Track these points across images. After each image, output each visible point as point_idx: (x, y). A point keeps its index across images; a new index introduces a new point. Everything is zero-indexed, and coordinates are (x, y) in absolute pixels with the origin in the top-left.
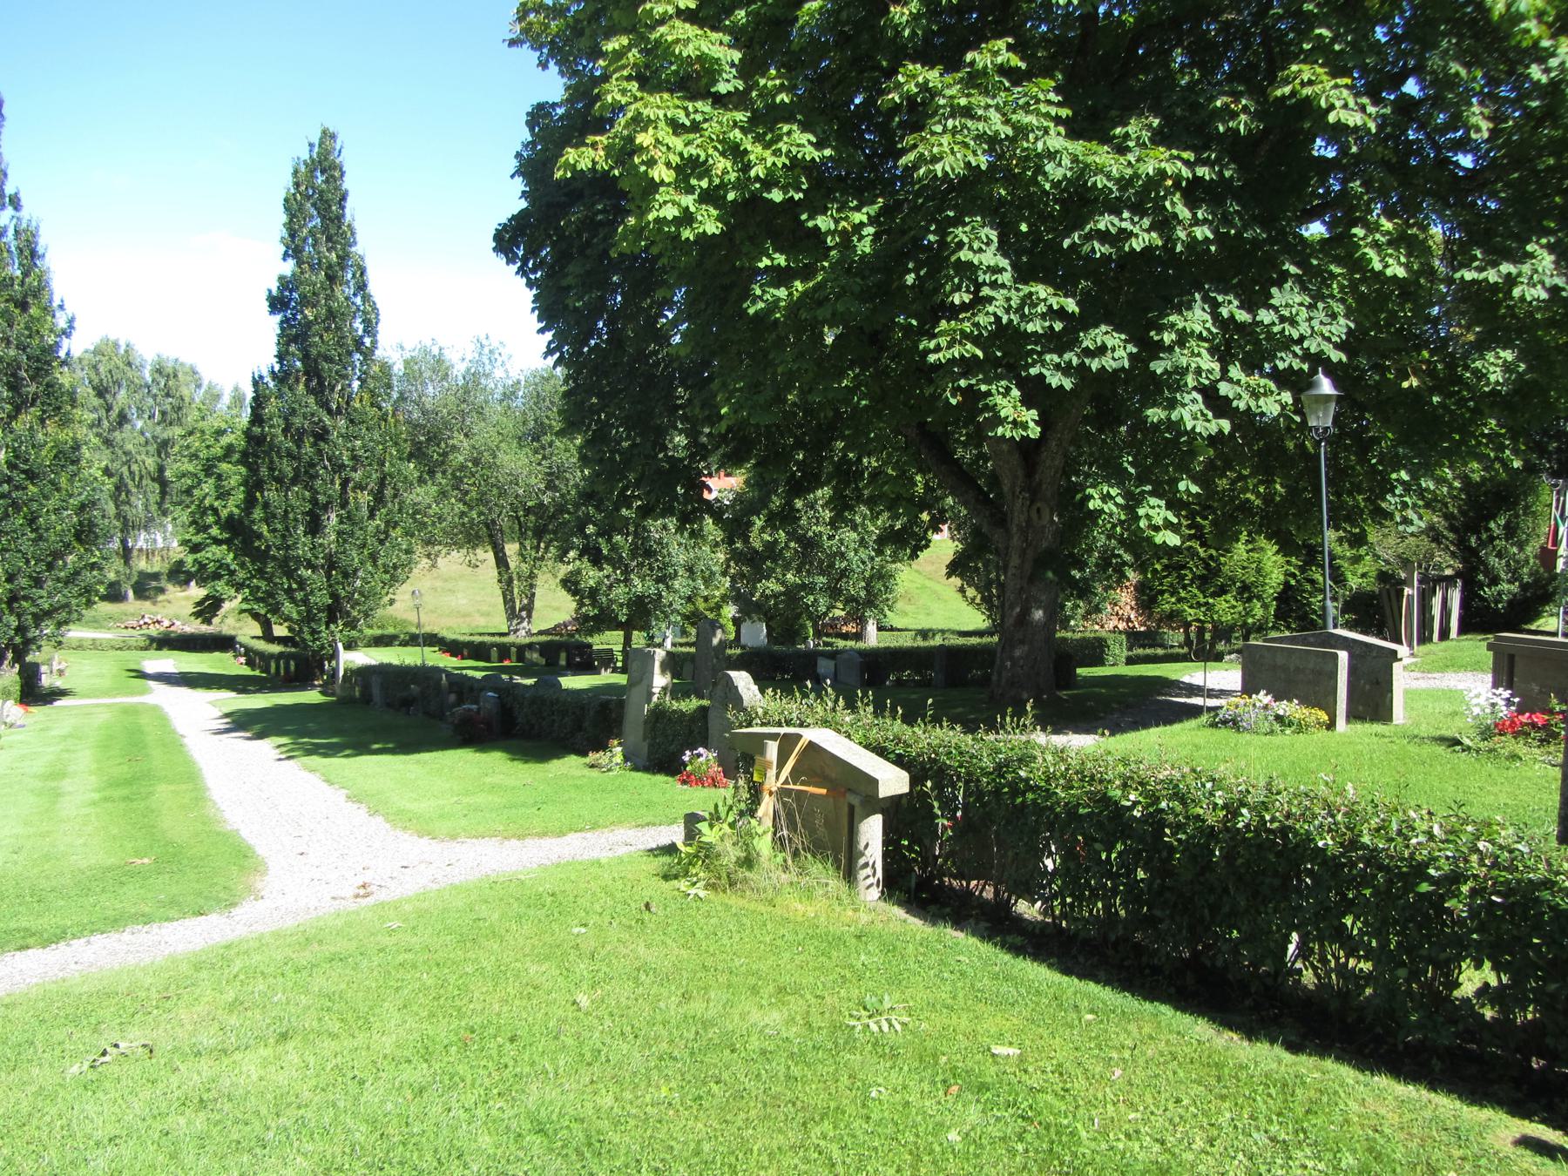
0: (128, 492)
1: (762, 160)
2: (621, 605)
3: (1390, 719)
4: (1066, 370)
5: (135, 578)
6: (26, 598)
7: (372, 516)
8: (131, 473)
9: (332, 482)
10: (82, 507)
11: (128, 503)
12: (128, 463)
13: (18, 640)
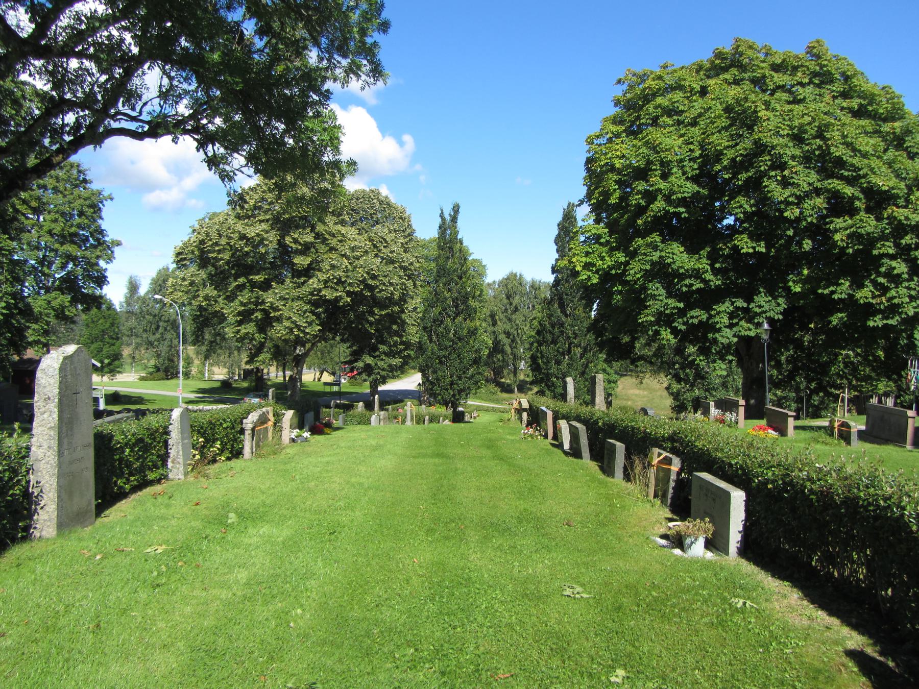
0: (517, 343)
1: (609, 262)
2: (689, 401)
3: (787, 435)
4: (684, 324)
5: (518, 383)
6: (456, 384)
7: (581, 358)
8: (518, 334)
9: (565, 344)
10: (476, 351)
11: (516, 347)
12: (517, 329)
13: (452, 399)
